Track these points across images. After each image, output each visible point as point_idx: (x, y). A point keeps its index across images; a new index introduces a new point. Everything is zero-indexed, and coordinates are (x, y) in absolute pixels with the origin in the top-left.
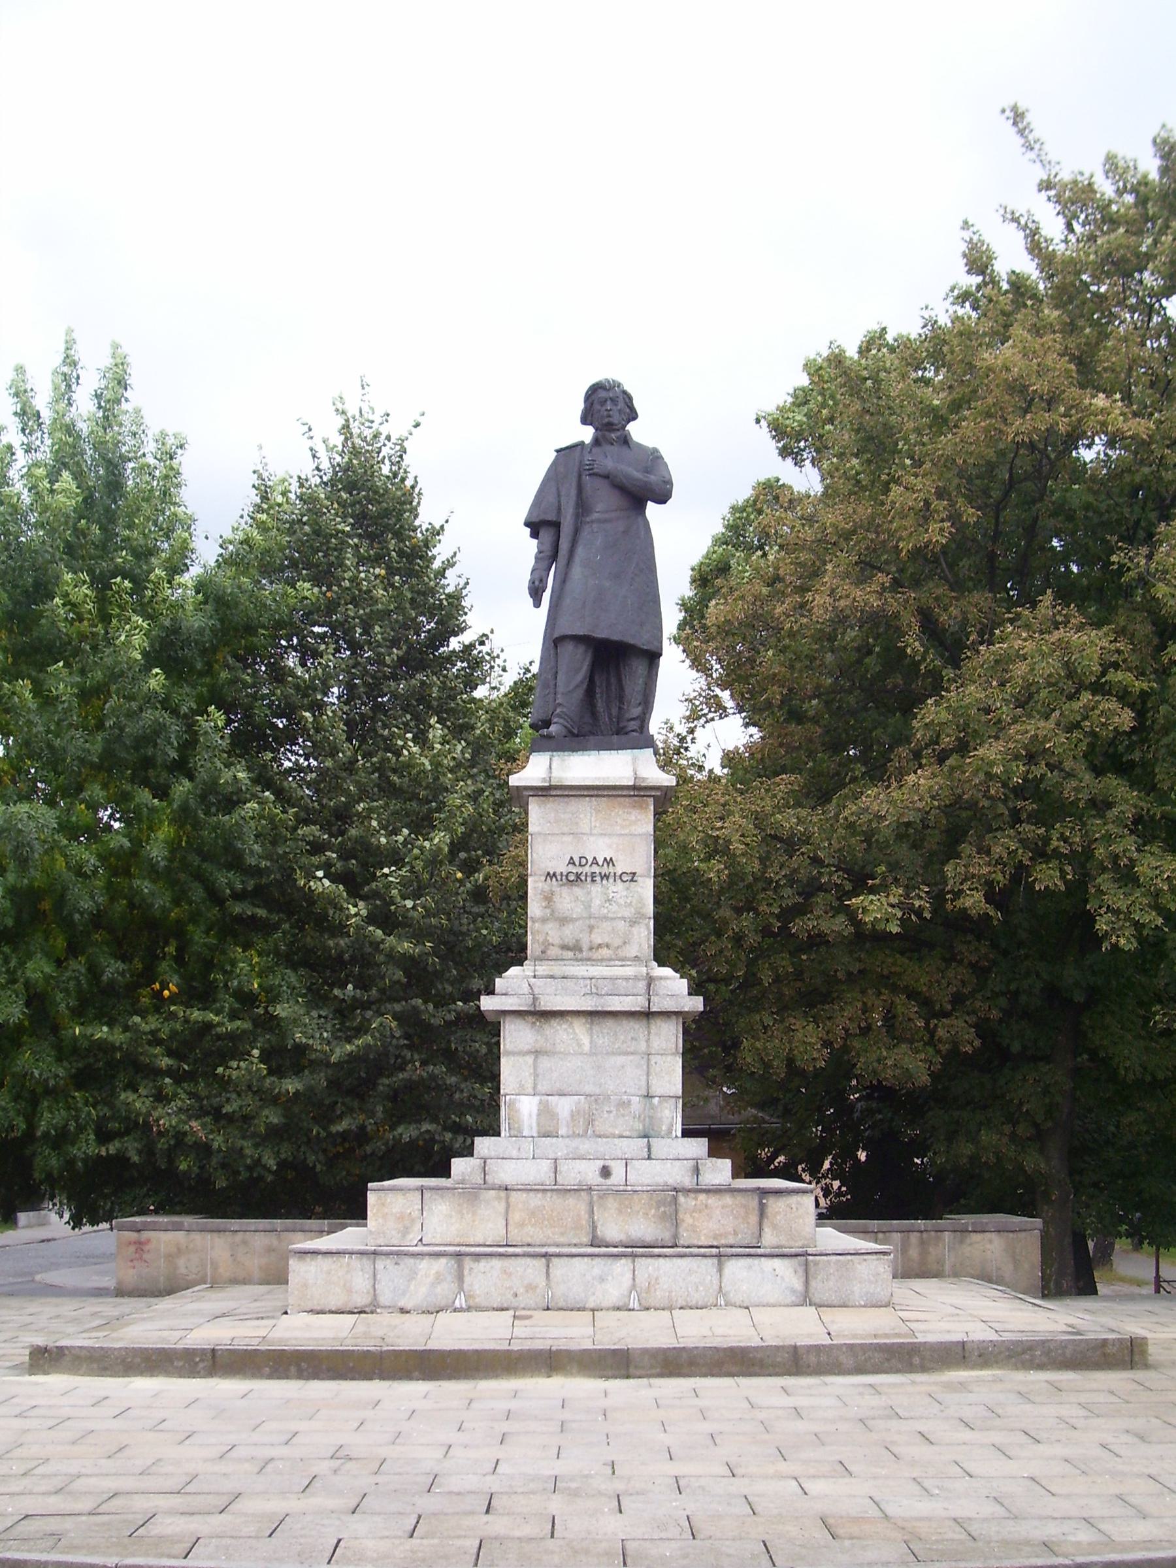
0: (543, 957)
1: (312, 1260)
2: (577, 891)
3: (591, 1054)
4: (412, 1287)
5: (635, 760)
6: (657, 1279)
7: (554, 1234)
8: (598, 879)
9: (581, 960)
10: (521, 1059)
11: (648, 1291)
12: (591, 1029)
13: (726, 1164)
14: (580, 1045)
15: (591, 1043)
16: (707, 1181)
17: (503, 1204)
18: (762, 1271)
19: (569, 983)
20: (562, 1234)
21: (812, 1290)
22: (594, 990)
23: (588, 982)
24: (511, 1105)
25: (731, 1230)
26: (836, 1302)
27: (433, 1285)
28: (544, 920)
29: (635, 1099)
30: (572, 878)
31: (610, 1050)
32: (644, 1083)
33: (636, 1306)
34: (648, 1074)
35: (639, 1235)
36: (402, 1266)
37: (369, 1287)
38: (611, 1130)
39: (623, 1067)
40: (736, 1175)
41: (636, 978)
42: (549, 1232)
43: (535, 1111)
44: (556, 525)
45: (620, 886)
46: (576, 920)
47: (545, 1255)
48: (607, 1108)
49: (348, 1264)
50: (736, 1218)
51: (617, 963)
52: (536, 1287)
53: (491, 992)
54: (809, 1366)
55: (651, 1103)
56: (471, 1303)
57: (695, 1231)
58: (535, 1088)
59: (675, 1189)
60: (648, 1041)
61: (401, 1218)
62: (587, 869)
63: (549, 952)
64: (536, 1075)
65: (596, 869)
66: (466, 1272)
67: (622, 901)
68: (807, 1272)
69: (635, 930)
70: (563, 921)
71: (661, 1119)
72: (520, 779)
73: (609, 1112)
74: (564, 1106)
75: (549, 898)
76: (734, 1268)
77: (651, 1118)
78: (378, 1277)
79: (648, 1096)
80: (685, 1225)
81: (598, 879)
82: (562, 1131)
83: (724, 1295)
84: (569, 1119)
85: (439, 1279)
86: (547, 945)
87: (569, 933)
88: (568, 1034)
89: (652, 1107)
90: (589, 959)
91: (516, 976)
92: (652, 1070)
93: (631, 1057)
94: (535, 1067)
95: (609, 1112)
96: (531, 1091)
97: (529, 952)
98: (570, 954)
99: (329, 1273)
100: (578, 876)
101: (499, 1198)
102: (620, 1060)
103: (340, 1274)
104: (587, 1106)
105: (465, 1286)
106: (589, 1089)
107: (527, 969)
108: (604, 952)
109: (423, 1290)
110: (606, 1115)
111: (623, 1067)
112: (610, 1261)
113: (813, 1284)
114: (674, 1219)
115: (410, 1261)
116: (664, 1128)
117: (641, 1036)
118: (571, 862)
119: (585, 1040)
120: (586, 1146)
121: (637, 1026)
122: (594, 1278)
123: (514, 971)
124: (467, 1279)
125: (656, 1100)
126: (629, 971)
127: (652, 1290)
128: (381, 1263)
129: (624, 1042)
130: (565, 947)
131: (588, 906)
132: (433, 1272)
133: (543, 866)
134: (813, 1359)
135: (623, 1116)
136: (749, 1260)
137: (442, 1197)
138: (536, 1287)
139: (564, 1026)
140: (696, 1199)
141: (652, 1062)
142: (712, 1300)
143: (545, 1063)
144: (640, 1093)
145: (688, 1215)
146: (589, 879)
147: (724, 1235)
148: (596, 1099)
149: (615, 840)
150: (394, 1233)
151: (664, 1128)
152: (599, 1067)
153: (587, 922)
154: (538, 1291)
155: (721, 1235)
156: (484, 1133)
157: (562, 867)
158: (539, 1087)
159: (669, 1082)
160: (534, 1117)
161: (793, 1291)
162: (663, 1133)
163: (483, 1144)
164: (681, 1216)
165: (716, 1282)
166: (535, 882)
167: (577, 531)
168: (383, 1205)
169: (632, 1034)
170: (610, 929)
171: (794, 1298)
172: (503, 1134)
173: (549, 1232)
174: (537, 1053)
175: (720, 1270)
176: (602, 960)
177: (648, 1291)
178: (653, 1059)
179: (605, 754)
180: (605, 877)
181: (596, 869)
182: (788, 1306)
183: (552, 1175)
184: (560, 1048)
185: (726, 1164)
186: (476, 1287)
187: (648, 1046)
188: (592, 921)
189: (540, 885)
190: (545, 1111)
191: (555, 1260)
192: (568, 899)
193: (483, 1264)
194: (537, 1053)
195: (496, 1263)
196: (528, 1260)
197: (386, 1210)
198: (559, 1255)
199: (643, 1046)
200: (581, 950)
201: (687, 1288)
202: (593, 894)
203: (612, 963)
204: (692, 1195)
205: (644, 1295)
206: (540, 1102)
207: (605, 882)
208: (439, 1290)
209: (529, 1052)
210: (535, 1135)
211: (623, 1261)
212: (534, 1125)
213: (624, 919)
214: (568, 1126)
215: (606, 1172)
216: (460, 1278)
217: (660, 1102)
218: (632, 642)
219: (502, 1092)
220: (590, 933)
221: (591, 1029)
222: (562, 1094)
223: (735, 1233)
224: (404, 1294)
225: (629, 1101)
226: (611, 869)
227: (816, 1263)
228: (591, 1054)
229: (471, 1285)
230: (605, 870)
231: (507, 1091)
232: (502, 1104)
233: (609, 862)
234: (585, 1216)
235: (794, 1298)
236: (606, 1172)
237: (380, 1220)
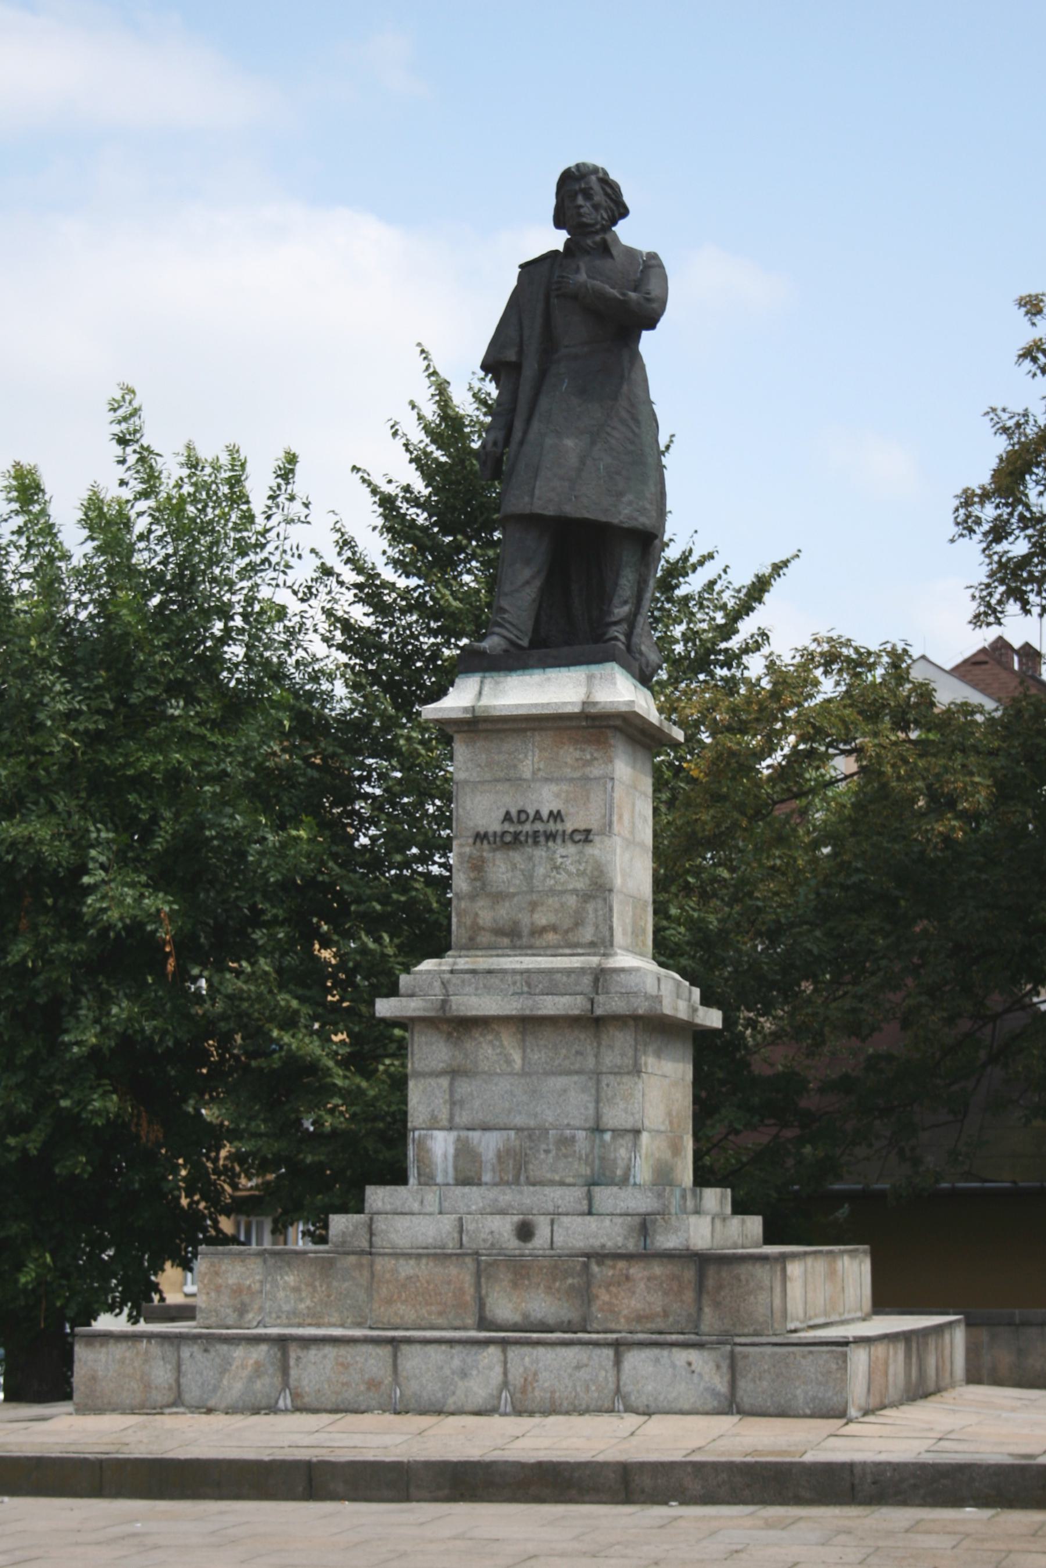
0: (471, 946)
1: (102, 1345)
2: (516, 856)
3: (524, 1074)
4: (225, 1382)
5: (590, 678)
6: (535, 1374)
7: (430, 1313)
8: (542, 839)
9: (521, 948)
10: (432, 1081)
11: (524, 1391)
12: (523, 1040)
13: (755, 1224)
14: (509, 1062)
15: (524, 1059)
16: (657, 1244)
17: (366, 1273)
18: (674, 1366)
19: (494, 980)
20: (440, 1314)
21: (740, 1393)
22: (525, 989)
23: (518, 977)
24: (421, 1144)
25: (659, 1309)
26: (772, 1410)
27: (251, 1380)
28: (473, 897)
29: (581, 1135)
30: (508, 838)
31: (548, 1068)
32: (591, 1112)
33: (509, 1409)
34: (597, 1101)
35: (539, 1316)
36: (213, 1353)
37: (172, 1381)
38: (549, 1176)
39: (565, 1091)
40: (769, 1238)
41: (582, 971)
42: (424, 1312)
43: (451, 1151)
44: (516, 368)
45: (571, 849)
46: (514, 895)
47: (392, 1341)
48: (544, 1146)
49: (147, 1352)
50: (666, 1294)
51: (568, 951)
52: (380, 1383)
53: (393, 991)
54: (643, 1491)
55: (602, 1140)
56: (299, 1403)
57: (612, 1311)
58: (451, 1119)
59: (588, 1256)
60: (596, 1056)
61: (237, 1291)
62: (527, 827)
63: (479, 939)
64: (453, 1103)
65: (539, 826)
66: (292, 1362)
67: (572, 869)
68: (733, 1368)
69: (590, 907)
70: (499, 897)
71: (615, 1160)
72: (441, 709)
73: (547, 1152)
74: (489, 1144)
75: (477, 867)
76: (635, 1360)
77: (602, 1159)
78: (183, 1368)
79: (597, 1129)
80: (599, 1302)
81: (542, 839)
82: (487, 1177)
83: (624, 1398)
84: (495, 1161)
85: (258, 1371)
86: (476, 929)
87: (504, 912)
88: (494, 1047)
89: (603, 1145)
90: (531, 947)
91: (428, 972)
92: (603, 1095)
93: (575, 1078)
94: (452, 1091)
95: (547, 1152)
96: (445, 1123)
97: (454, 939)
98: (506, 941)
99: (122, 1361)
100: (516, 835)
101: (360, 1266)
102: (561, 1082)
103: (136, 1364)
104: (517, 1143)
105: (292, 1383)
106: (519, 1120)
107: (445, 964)
108: (551, 937)
109: (239, 1386)
110: (543, 1156)
111: (565, 1091)
112: (474, 1349)
113: (742, 1384)
114: (585, 1294)
115: (224, 1348)
116: (619, 1172)
117: (589, 1048)
118: (507, 817)
119: (517, 1057)
120: (506, 1196)
121: (582, 1036)
122: (453, 1373)
123: (428, 965)
124: (293, 1373)
125: (608, 1136)
126: (576, 962)
127: (530, 1389)
128: (186, 1352)
129: (566, 1057)
130: (499, 932)
131: (529, 877)
132: (251, 1362)
133: (471, 824)
134: (647, 1482)
135: (566, 1156)
136: (655, 1352)
137: (289, 1264)
138: (380, 1383)
139: (490, 1037)
140: (614, 1267)
141: (604, 1084)
142: (607, 1405)
143: (464, 1087)
144: (587, 1125)
145: (603, 1291)
146: (530, 841)
147: (649, 1318)
148: (533, 1134)
149: (565, 787)
150: (229, 1311)
151: (619, 1172)
152: (535, 1091)
153: (528, 898)
154: (383, 1387)
155: (647, 1317)
156: (383, 1181)
157: (495, 825)
158: (457, 1119)
159: (626, 1111)
160: (451, 1159)
161: (715, 1393)
162: (617, 1180)
163: (377, 1196)
164: (595, 1290)
165: (612, 1379)
166: (461, 846)
167: (542, 375)
168: (217, 1274)
169: (576, 1047)
170: (557, 906)
171: (715, 1404)
172: (412, 1180)
173: (424, 1312)
174: (454, 1073)
175: (618, 1362)
176: (548, 947)
177: (524, 1391)
178: (605, 1080)
179: (553, 673)
180: (551, 836)
181: (539, 826)
182: (707, 1413)
183: (456, 1235)
184: (484, 1066)
185: (755, 1224)
186: (305, 1383)
187: (598, 1063)
188: (535, 897)
189: (467, 850)
190: (464, 1152)
191: (405, 1348)
192: (503, 869)
193: (313, 1354)
194: (454, 1073)
195: (330, 1351)
196: (370, 1349)
197: (220, 1281)
198: (409, 1341)
199: (590, 1062)
200: (520, 936)
201: (574, 1387)
202: (537, 860)
203: (561, 951)
204: (609, 1262)
205: (518, 1395)
206: (458, 1139)
207: (550, 844)
208: (258, 1385)
209: (442, 1073)
210: (451, 1181)
211: (492, 1350)
212: (451, 1170)
213: (575, 891)
214: (493, 1170)
215: (525, 1232)
216: (285, 1370)
217: (613, 1138)
218: (603, 518)
219: (409, 1125)
220: (532, 911)
221: (523, 1040)
222: (486, 1128)
223: (666, 1314)
224: (215, 1389)
225: (574, 1137)
226: (559, 827)
227: (746, 1357)
228: (524, 1074)
229: (299, 1380)
230: (552, 826)
231: (416, 1124)
232: (410, 1141)
233: (556, 816)
234: (470, 1290)
235: (715, 1404)
236: (525, 1232)
237: (213, 1295)
